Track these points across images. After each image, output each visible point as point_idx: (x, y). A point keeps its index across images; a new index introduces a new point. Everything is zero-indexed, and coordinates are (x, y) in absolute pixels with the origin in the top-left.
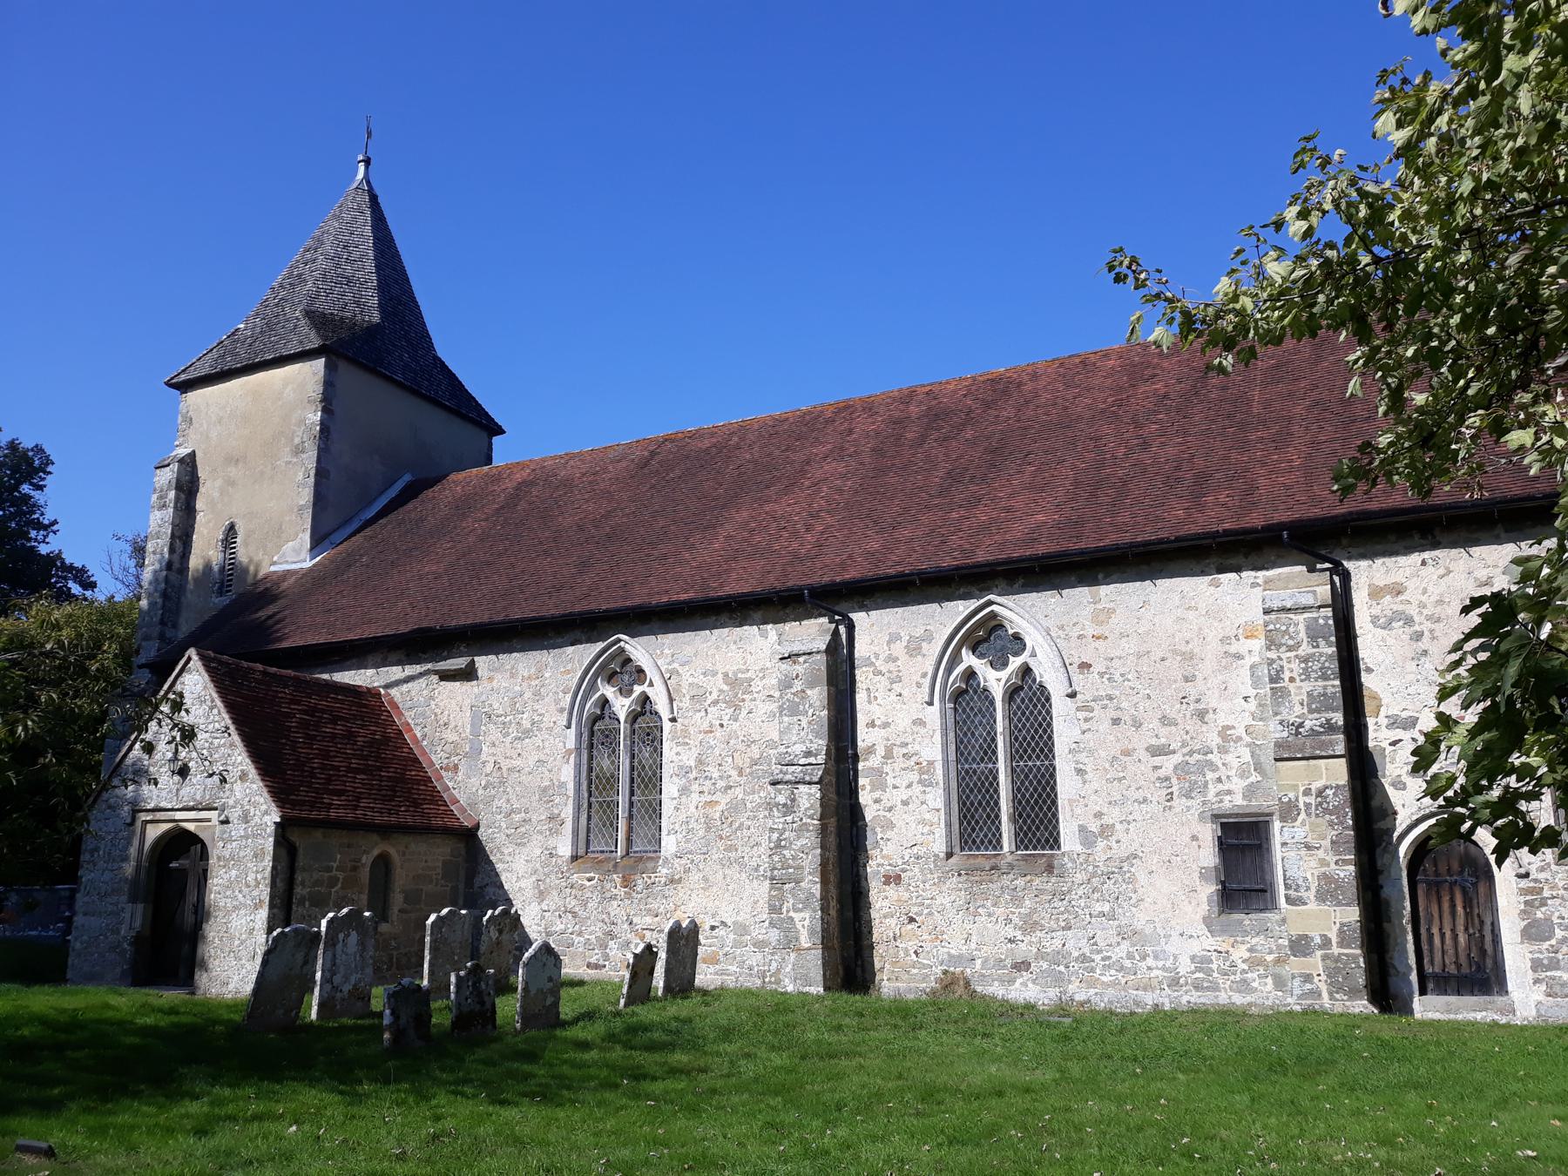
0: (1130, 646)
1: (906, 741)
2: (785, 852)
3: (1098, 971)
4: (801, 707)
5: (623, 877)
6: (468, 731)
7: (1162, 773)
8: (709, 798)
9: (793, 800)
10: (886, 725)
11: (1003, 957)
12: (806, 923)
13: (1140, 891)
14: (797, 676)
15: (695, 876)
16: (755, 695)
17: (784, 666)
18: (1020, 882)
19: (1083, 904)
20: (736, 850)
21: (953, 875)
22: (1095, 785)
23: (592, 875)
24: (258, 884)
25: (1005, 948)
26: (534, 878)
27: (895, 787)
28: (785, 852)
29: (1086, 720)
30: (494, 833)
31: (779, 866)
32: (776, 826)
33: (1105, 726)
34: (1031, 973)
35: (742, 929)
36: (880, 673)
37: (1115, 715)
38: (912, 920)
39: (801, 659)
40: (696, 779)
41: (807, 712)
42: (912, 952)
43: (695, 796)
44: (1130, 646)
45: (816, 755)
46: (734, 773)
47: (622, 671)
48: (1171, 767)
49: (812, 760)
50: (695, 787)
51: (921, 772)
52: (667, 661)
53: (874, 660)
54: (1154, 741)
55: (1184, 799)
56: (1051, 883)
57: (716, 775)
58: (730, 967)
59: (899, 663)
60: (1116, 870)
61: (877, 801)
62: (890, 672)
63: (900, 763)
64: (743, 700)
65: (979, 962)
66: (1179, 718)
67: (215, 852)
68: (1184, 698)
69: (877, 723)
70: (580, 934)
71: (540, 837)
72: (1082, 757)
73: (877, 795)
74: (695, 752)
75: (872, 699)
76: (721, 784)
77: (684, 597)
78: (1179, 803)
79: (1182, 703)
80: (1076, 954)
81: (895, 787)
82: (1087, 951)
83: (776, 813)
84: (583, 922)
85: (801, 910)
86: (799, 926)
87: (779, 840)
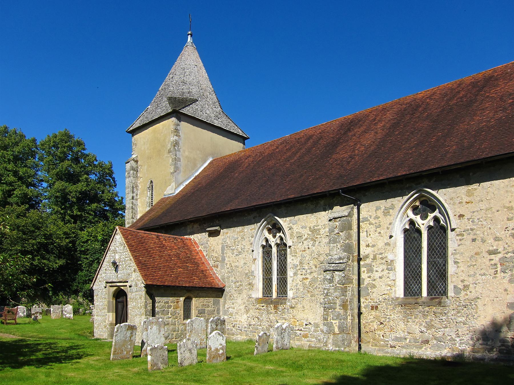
0: (483, 206)
1: (382, 252)
2: (330, 297)
3: (458, 345)
4: (338, 240)
5: (274, 306)
6: (221, 252)
7: (493, 262)
8: (304, 277)
9: (333, 277)
10: (373, 246)
11: (418, 338)
12: (337, 324)
13: (479, 312)
14: (336, 227)
15: (299, 306)
16: (322, 236)
17: (331, 223)
18: (427, 309)
19: (453, 318)
20: (315, 296)
21: (399, 306)
22: (462, 268)
23: (264, 305)
24: (141, 307)
25: (419, 335)
26: (244, 305)
27: (377, 271)
28: (330, 297)
29: (460, 240)
30: (230, 289)
31: (327, 303)
32: (326, 288)
33: (468, 242)
34: (429, 345)
35: (317, 326)
36: (372, 224)
37: (474, 237)
38: (382, 323)
39: (338, 220)
40: (299, 269)
41: (340, 242)
42: (381, 336)
43: (299, 276)
44: (483, 206)
45: (343, 259)
46: (314, 267)
47: (276, 228)
48: (497, 259)
49: (341, 261)
50: (299, 272)
51: (388, 265)
52: (288, 223)
53: (369, 219)
54: (491, 248)
55: (502, 273)
56: (439, 310)
57: (306, 268)
58: (312, 339)
59: (380, 219)
60: (469, 304)
61: (369, 277)
62: (376, 223)
63: (379, 261)
64: (317, 238)
65: (408, 340)
66: (503, 237)
67: (129, 296)
68: (506, 228)
69: (370, 245)
70: (260, 325)
71: (245, 291)
72: (457, 256)
73: (369, 275)
74: (299, 259)
75: (368, 235)
76: (309, 271)
77: (292, 196)
78: (500, 275)
79: (505, 230)
80: (449, 338)
81: (377, 271)
82: (454, 336)
83: (326, 283)
84: (261, 321)
85: (335, 320)
86: (335, 325)
87: (327, 293)
